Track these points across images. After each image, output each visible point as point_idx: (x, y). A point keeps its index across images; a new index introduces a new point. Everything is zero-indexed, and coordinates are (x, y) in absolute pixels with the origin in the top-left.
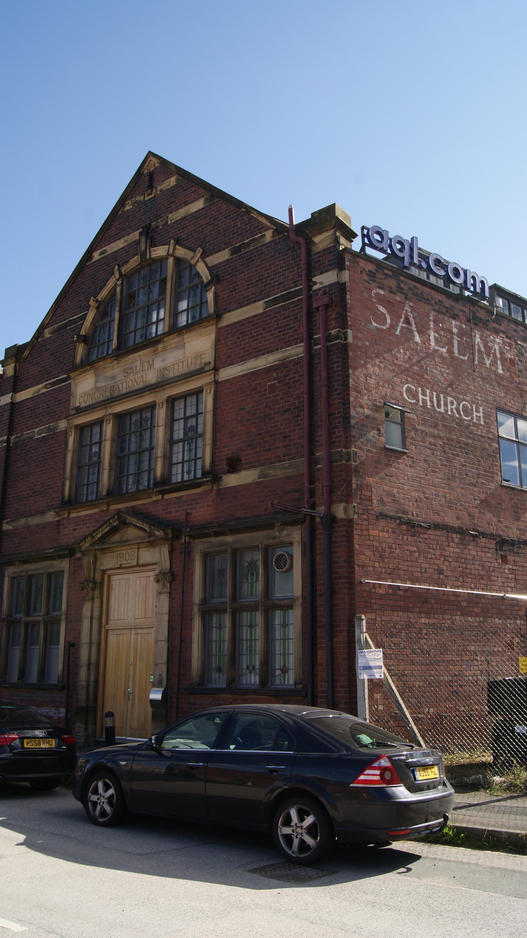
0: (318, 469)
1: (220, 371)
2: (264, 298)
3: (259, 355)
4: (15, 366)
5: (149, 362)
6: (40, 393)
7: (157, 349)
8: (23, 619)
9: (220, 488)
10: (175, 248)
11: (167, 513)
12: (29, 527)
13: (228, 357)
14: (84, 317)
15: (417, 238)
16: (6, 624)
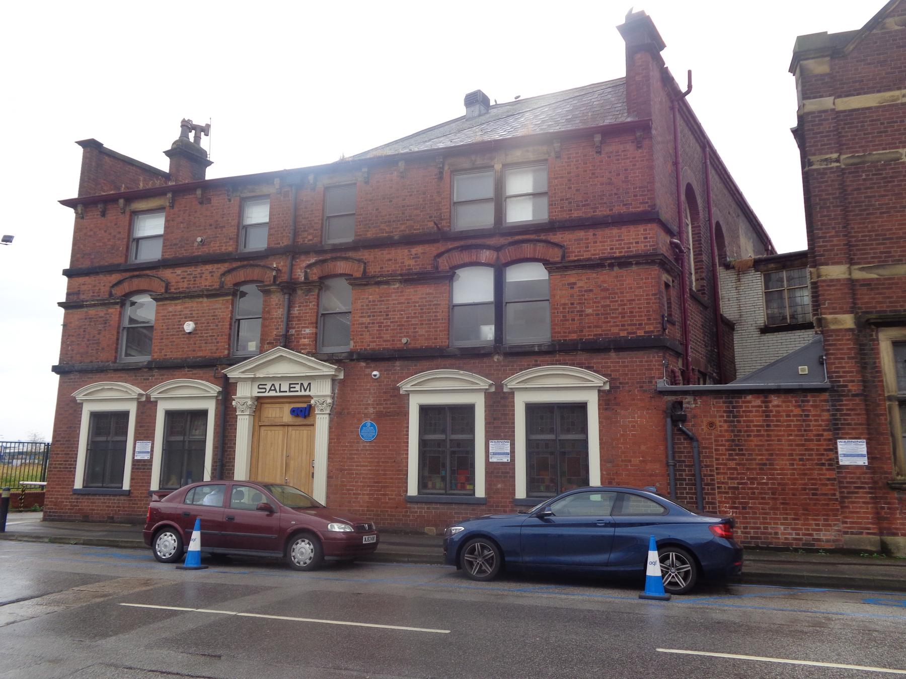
6: (899, 102)
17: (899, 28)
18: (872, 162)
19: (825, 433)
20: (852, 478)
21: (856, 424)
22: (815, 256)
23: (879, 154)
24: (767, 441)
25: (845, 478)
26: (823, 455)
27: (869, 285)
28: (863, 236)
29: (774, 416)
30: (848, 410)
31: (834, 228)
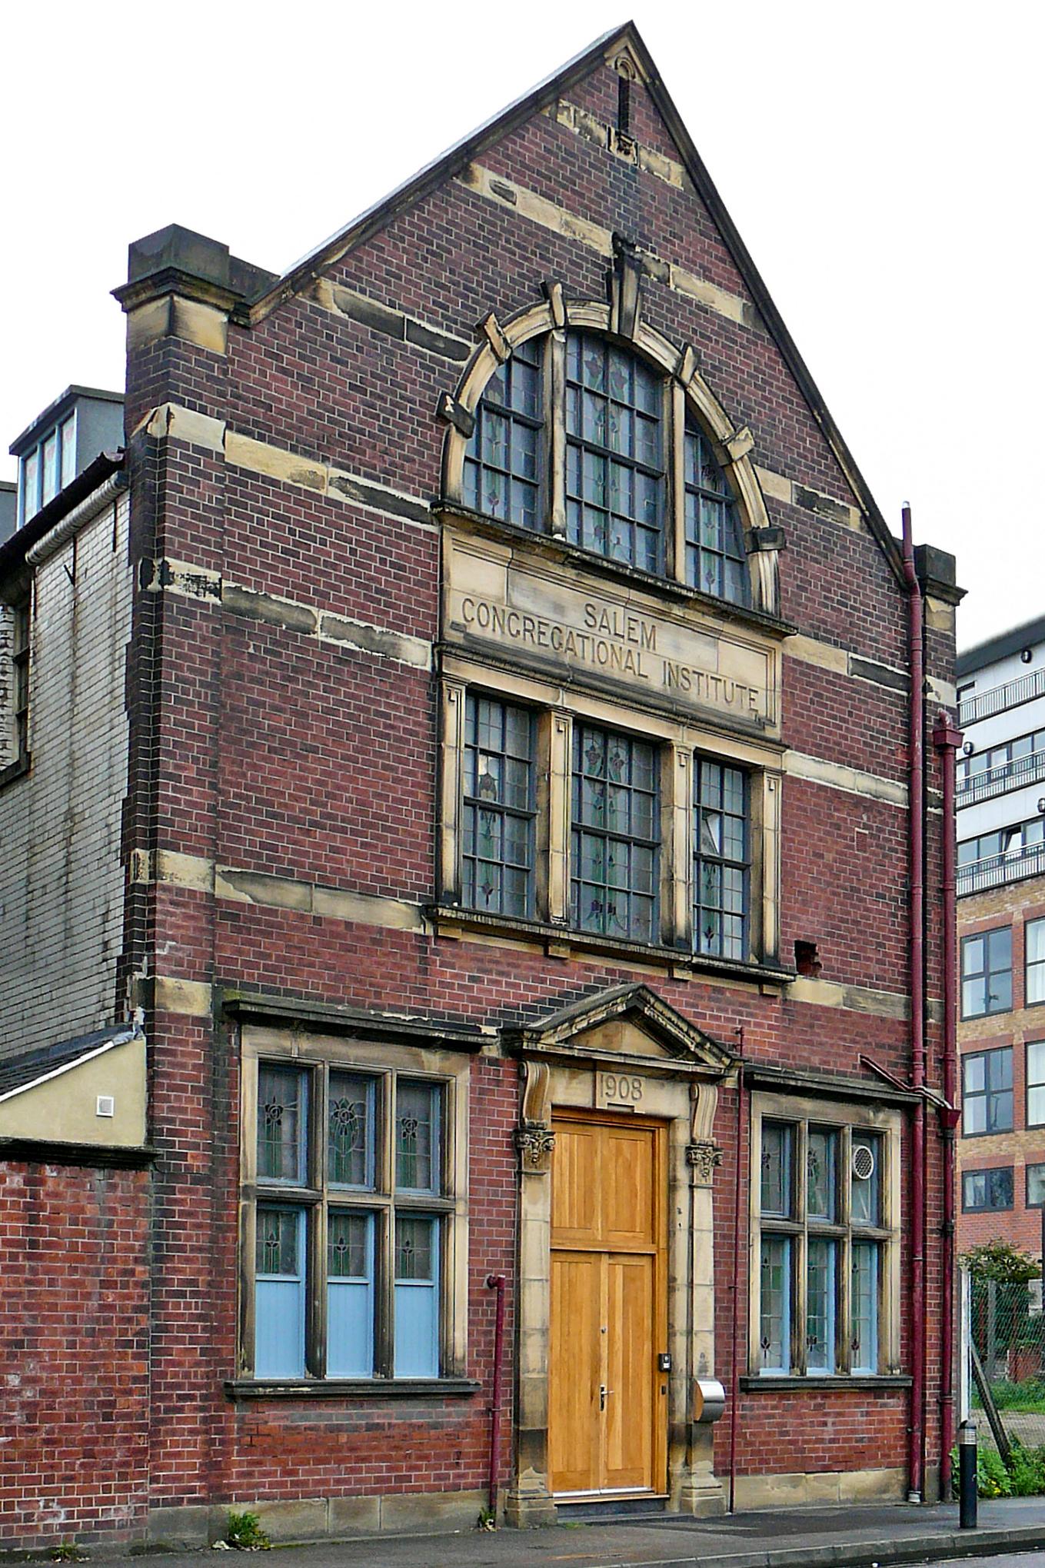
12: (318, 920)
15: (177, 237)
17: (339, 313)
19: (139, 1268)
20: (175, 1375)
21: (193, 1249)
22: (155, 821)
23: (280, 604)
24: (28, 1282)
25: (164, 1375)
26: (129, 1320)
27: (235, 917)
29: (48, 1220)
30: (182, 1214)
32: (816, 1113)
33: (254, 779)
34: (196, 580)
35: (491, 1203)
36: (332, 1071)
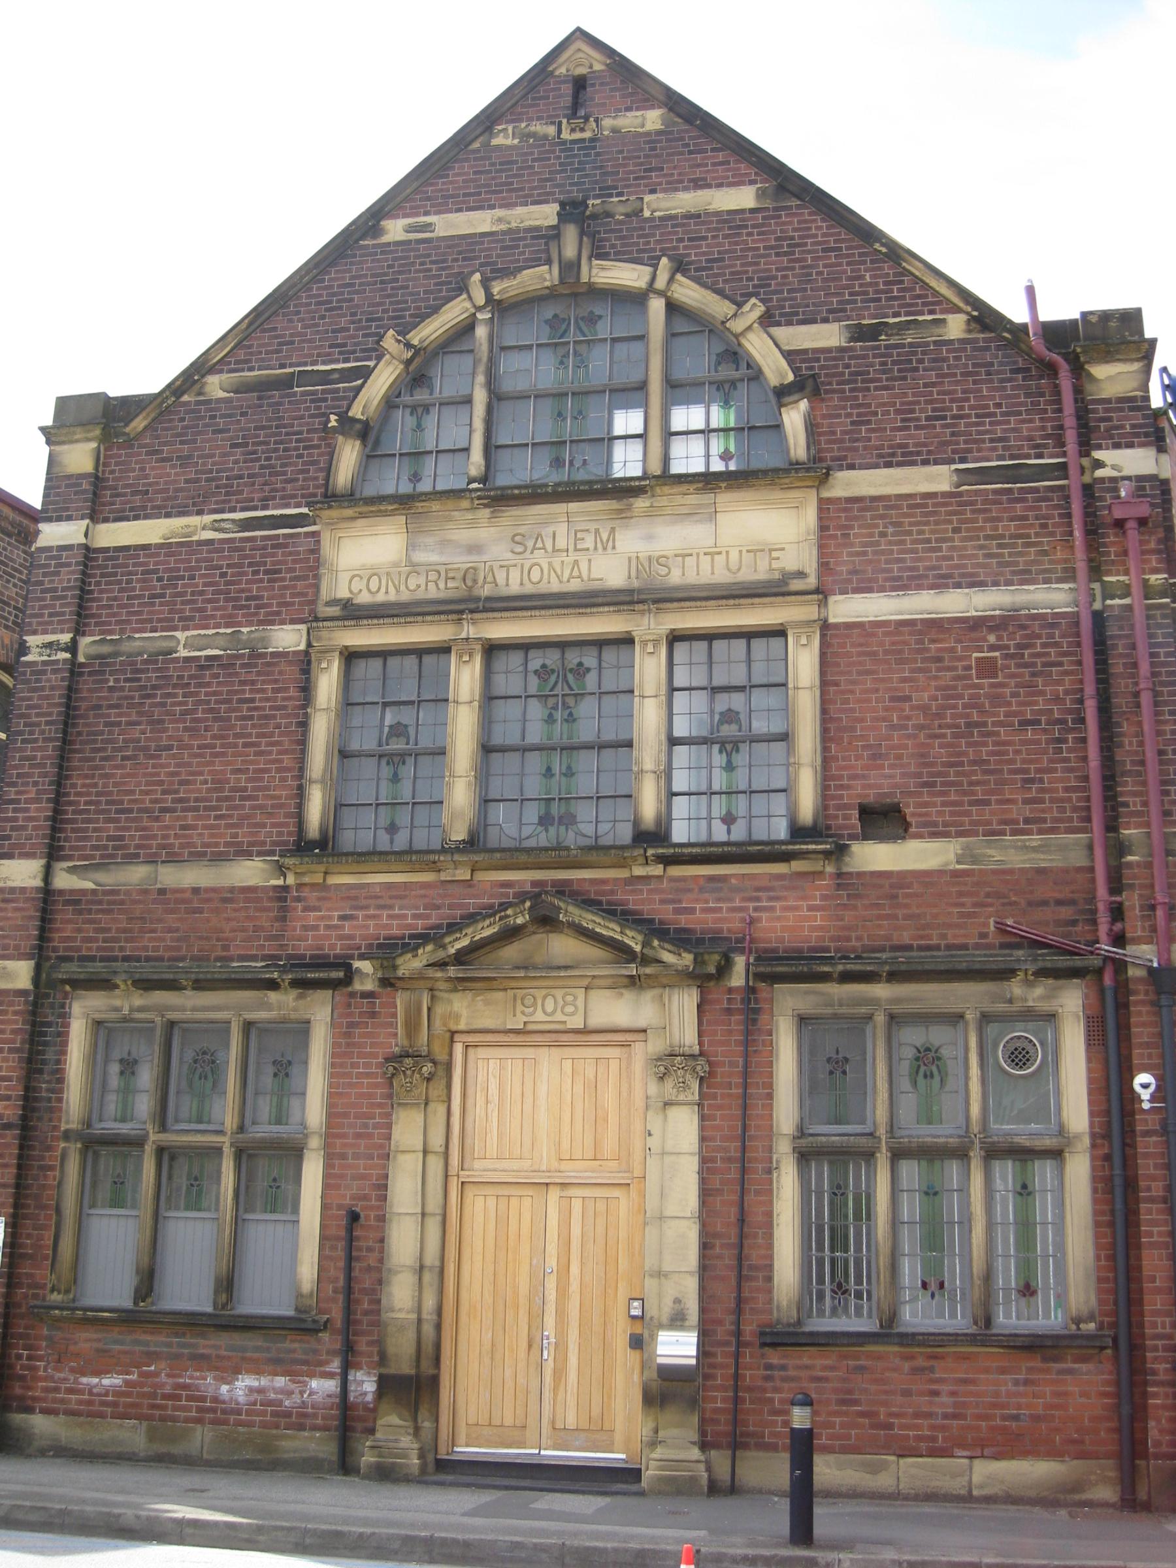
0: (1130, 865)
1: (832, 599)
2: (952, 461)
3: (946, 586)
4: (98, 448)
5: (597, 531)
6: (195, 538)
7: (629, 507)
8: (152, 1137)
9: (845, 869)
10: (671, 280)
11: (677, 911)
12: (162, 892)
13: (855, 572)
14: (365, 374)
16: (79, 1145)
18: (130, 655)
27: (78, 902)
28: (86, 803)
31: (36, 784)
32: (897, 1001)
33: (105, 785)
34: (49, 645)
35: (358, 1136)
36: (1121, 904)
